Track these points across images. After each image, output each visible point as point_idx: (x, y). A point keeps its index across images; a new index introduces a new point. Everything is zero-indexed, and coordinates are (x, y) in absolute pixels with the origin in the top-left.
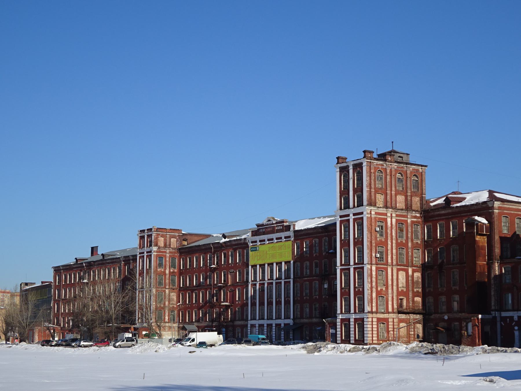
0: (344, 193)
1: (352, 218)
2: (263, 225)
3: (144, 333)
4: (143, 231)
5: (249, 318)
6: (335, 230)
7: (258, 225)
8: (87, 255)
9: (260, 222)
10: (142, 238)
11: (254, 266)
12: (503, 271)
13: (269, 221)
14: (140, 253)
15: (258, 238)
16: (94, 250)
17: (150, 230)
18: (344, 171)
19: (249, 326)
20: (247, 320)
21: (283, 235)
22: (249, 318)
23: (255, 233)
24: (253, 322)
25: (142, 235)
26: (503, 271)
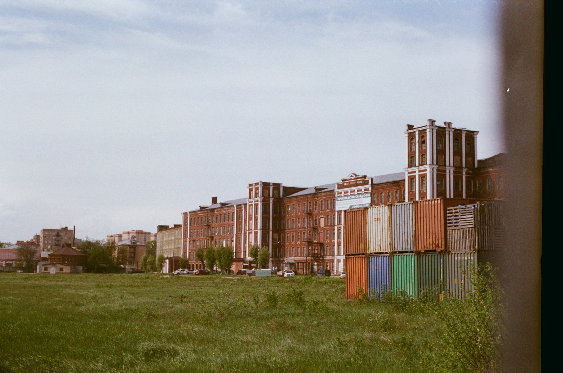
0: (411, 157)
1: (417, 174)
2: (346, 180)
3: (310, 248)
4: (250, 185)
5: (336, 254)
6: (404, 184)
7: (343, 180)
8: (208, 203)
9: (345, 178)
10: (251, 190)
11: (340, 212)
12: (224, 242)
13: (352, 176)
14: (249, 202)
15: (343, 190)
16: (214, 200)
17: (257, 184)
18: (411, 137)
19: (335, 260)
20: (333, 255)
21: (363, 188)
22: (336, 254)
23: (340, 186)
24: (339, 257)
25: (250, 187)
26: (224, 242)
